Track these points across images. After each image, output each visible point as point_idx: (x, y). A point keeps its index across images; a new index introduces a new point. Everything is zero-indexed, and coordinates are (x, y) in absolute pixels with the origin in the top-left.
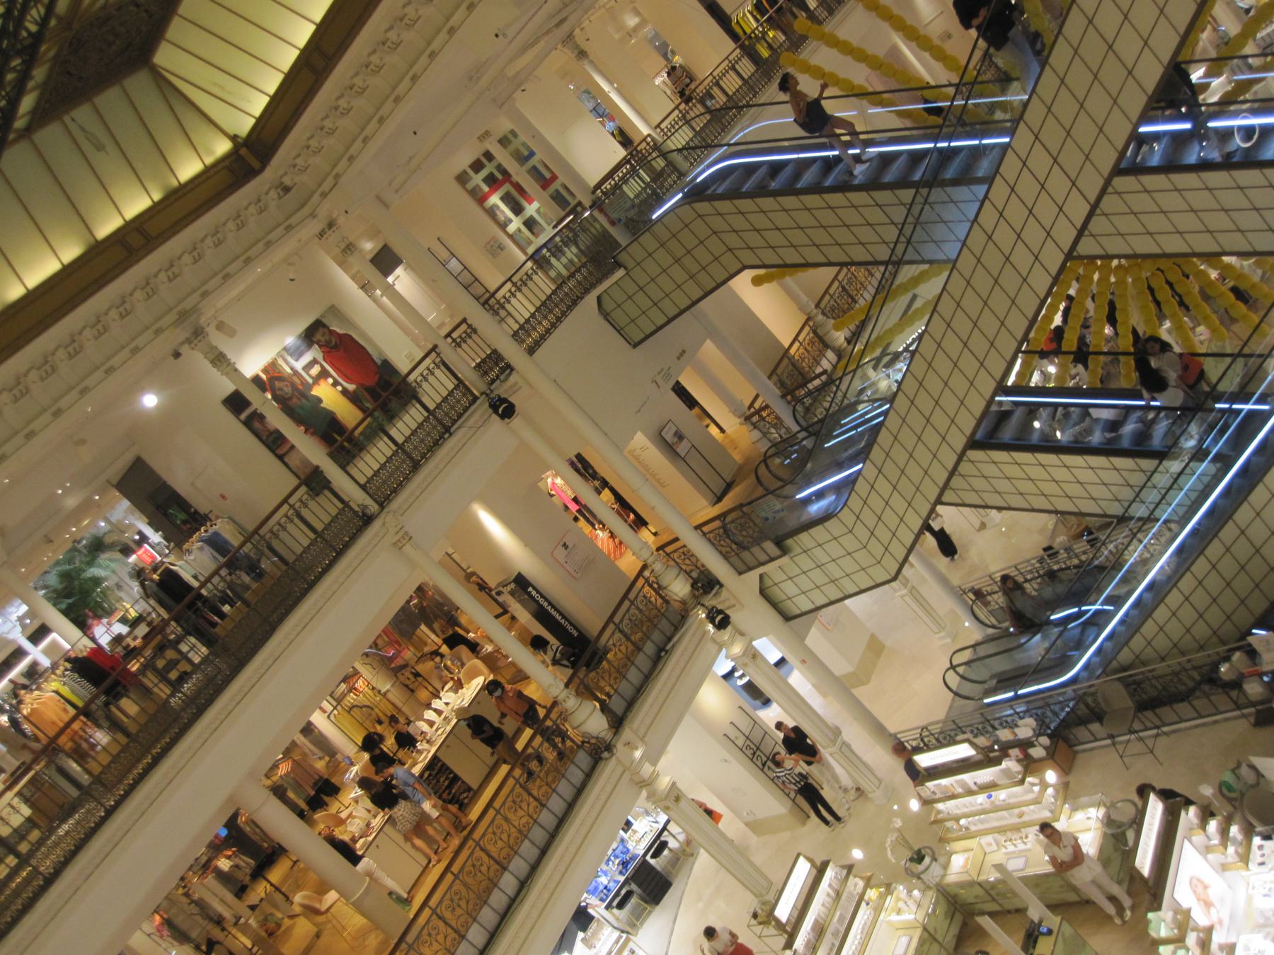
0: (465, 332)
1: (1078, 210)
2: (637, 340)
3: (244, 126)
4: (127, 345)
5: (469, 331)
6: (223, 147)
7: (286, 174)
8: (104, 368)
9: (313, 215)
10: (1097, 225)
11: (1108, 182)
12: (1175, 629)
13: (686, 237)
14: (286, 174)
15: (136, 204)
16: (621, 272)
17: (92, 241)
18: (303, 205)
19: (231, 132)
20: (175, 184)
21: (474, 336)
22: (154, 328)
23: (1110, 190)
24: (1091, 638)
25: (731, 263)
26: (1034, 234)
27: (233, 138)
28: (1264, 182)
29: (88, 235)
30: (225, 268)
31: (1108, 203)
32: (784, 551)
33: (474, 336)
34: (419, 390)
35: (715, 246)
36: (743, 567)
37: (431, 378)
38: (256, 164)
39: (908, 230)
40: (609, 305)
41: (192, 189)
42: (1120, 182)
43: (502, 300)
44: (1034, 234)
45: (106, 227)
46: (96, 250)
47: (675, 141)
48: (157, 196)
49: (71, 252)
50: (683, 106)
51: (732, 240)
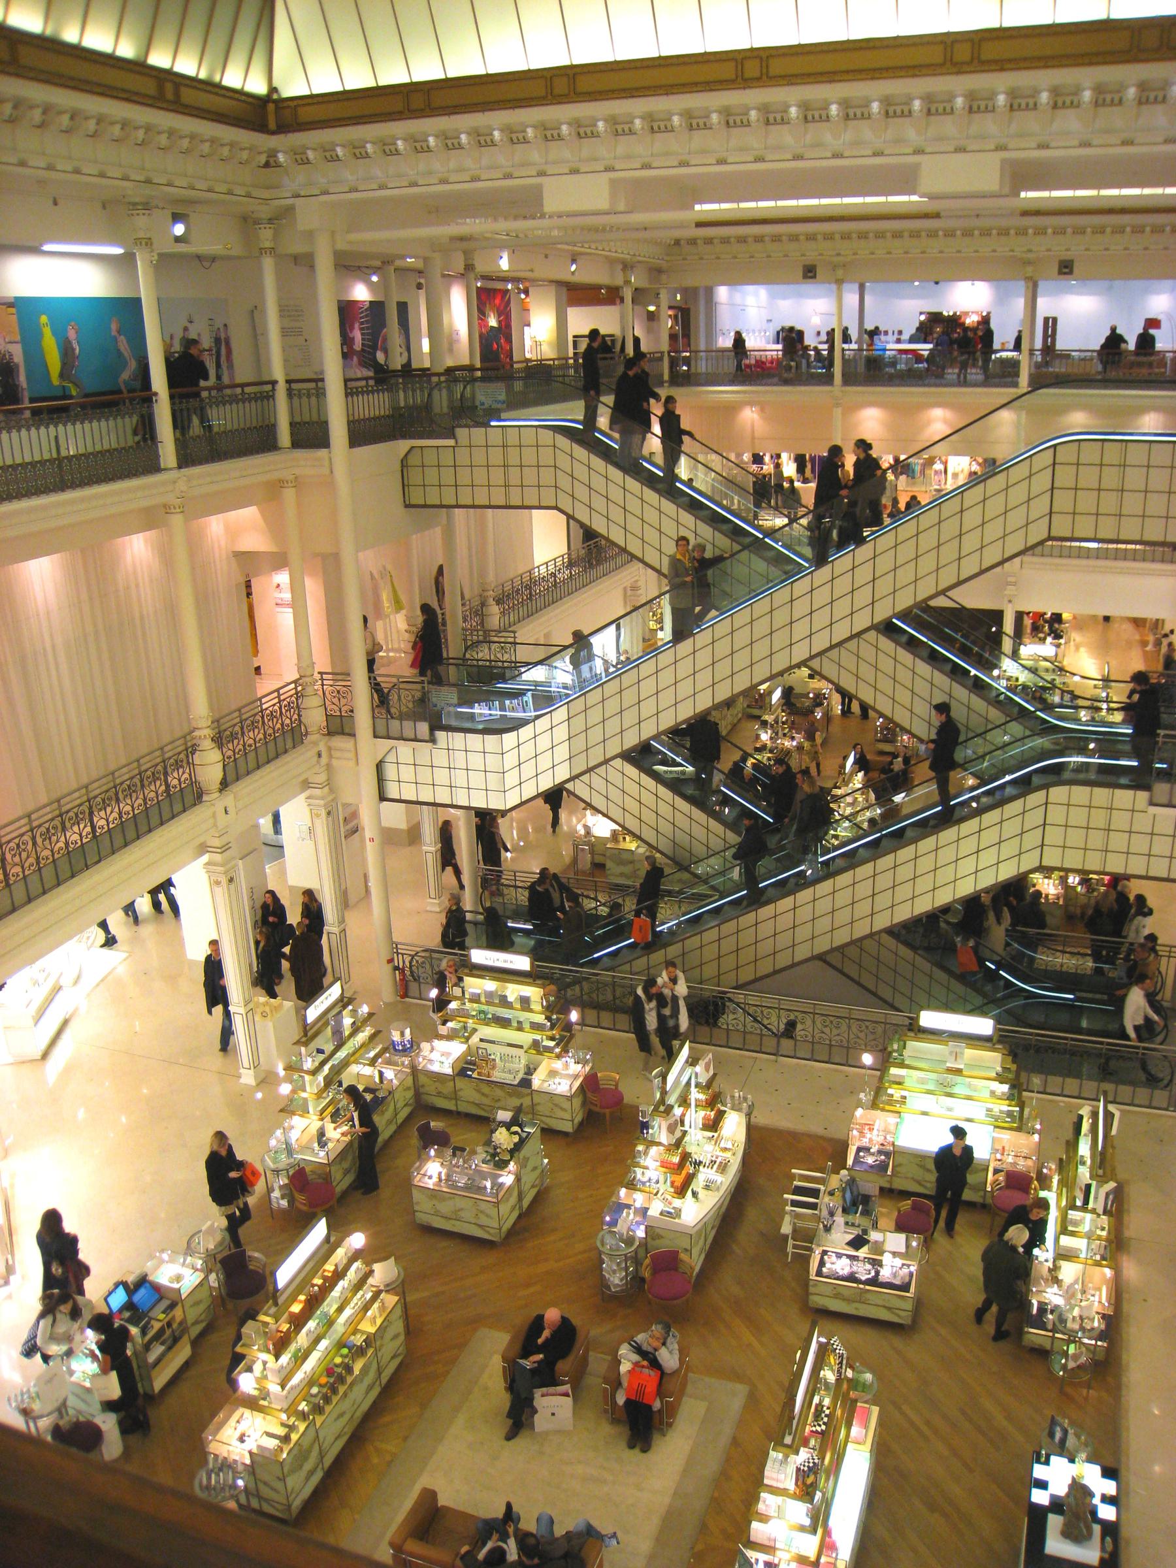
2: (413, 502)
3: (293, 87)
6: (257, 86)
15: (187, 65)
16: (451, 442)
17: (142, 59)
18: (268, 188)
19: (276, 83)
20: (217, 79)
21: (314, 400)
25: (548, 498)
27: (273, 90)
28: (929, 677)
29: (143, 51)
32: (433, 740)
33: (314, 400)
35: (547, 476)
36: (381, 730)
37: (305, 400)
38: (272, 125)
40: (414, 460)
41: (309, 104)
45: (159, 59)
46: (138, 67)
47: (305, 409)
48: (203, 75)
49: (127, 50)
50: (371, 382)
51: (564, 482)
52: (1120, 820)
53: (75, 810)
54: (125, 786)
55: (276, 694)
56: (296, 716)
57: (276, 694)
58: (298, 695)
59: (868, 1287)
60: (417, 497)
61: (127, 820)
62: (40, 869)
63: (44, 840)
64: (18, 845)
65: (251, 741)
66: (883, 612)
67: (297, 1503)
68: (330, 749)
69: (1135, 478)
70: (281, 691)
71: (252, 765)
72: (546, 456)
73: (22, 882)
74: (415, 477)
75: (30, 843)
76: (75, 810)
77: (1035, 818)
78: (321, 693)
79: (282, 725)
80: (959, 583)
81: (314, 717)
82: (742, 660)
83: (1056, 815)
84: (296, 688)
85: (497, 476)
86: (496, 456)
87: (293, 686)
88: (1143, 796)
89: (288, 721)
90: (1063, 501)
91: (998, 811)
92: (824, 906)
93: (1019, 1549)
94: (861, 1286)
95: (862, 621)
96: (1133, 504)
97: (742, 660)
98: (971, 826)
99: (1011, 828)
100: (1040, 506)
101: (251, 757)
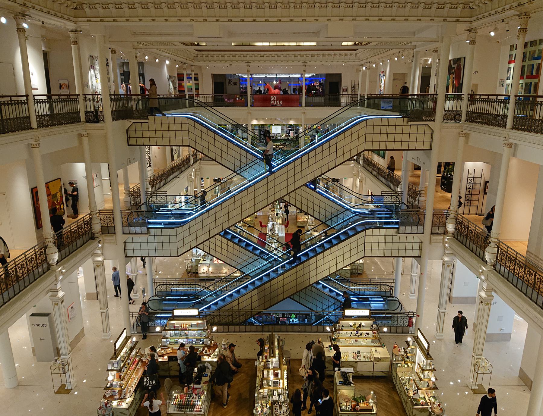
0: (8, 101)
1: (291, 188)
4: (41, 6)
5: (10, 102)
7: (86, 4)
8: (316, 18)
9: (75, 23)
10: (293, 194)
11: (302, 186)
12: (242, 306)
13: (178, 127)
14: (86, 4)
16: (147, 121)
22: (267, 18)
23: (301, 188)
24: (330, 284)
25: (153, 142)
26: (278, 188)
30: (181, 17)
31: (298, 191)
34: (426, 102)
39: (251, 164)
40: (133, 128)
42: (304, 188)
43: (13, 102)
44: (278, 188)
53: (21, 264)
54: (29, 259)
55: (33, 249)
56: (89, 228)
57: (33, 249)
58: (91, 219)
59: (360, 413)
60: (133, 142)
61: (30, 273)
62: (28, 274)
63: (30, 263)
64: (21, 265)
65: (31, 268)
68: (103, 239)
70: (85, 218)
71: (32, 279)
73: (23, 280)
74: (132, 134)
75: (35, 258)
76: (21, 264)
77: (361, 241)
78: (99, 217)
79: (85, 231)
81: (97, 228)
83: (368, 239)
84: (89, 217)
87: (88, 216)
89: (87, 230)
93: (385, 222)
94: (358, 413)
99: (354, 245)
101: (31, 275)
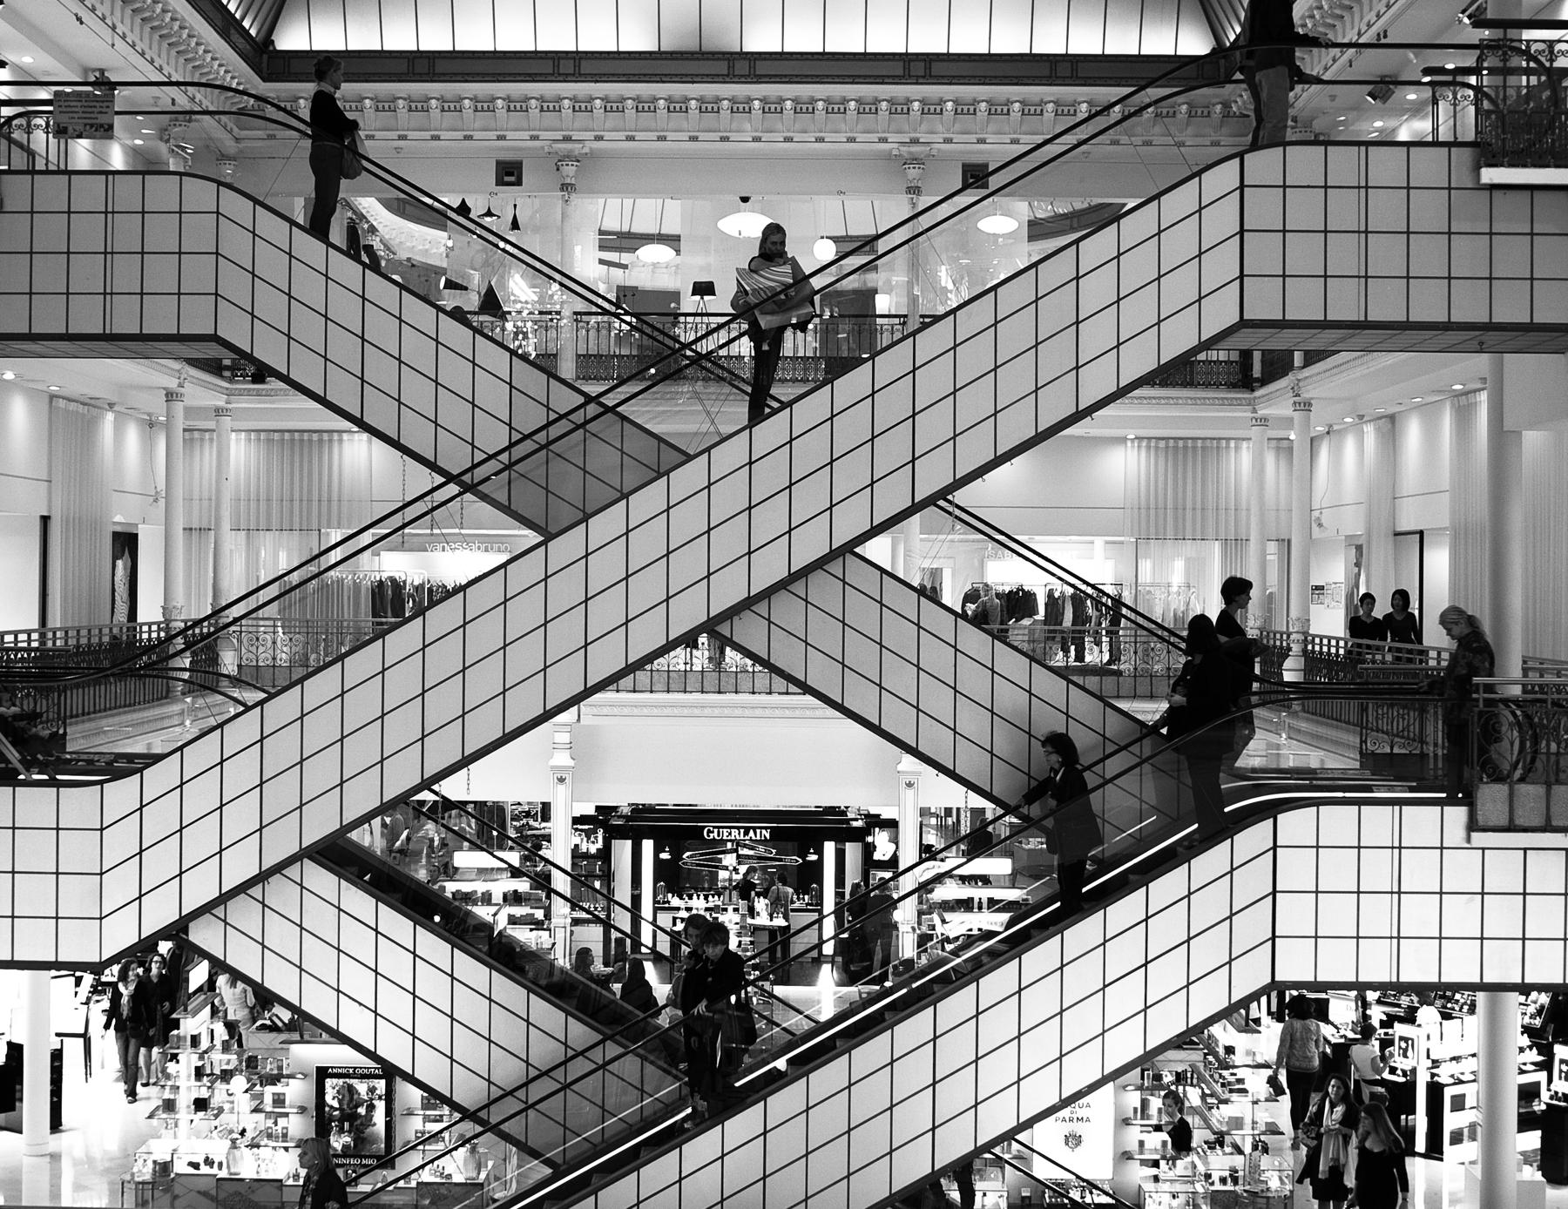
35: (198, 273)
52: (1420, 871)
66: (320, 825)
67: (1312, 556)
69: (1386, 210)
72: (199, 233)
77: (1253, 881)
80: (466, 762)
82: (322, 772)
85: (87, 273)
86: (88, 233)
88: (1457, 816)
90: (1264, 255)
91: (1179, 873)
92: (828, 1120)
95: (282, 844)
96: (1386, 255)
97: (322, 772)
98: (1126, 909)
100: (1222, 264)
